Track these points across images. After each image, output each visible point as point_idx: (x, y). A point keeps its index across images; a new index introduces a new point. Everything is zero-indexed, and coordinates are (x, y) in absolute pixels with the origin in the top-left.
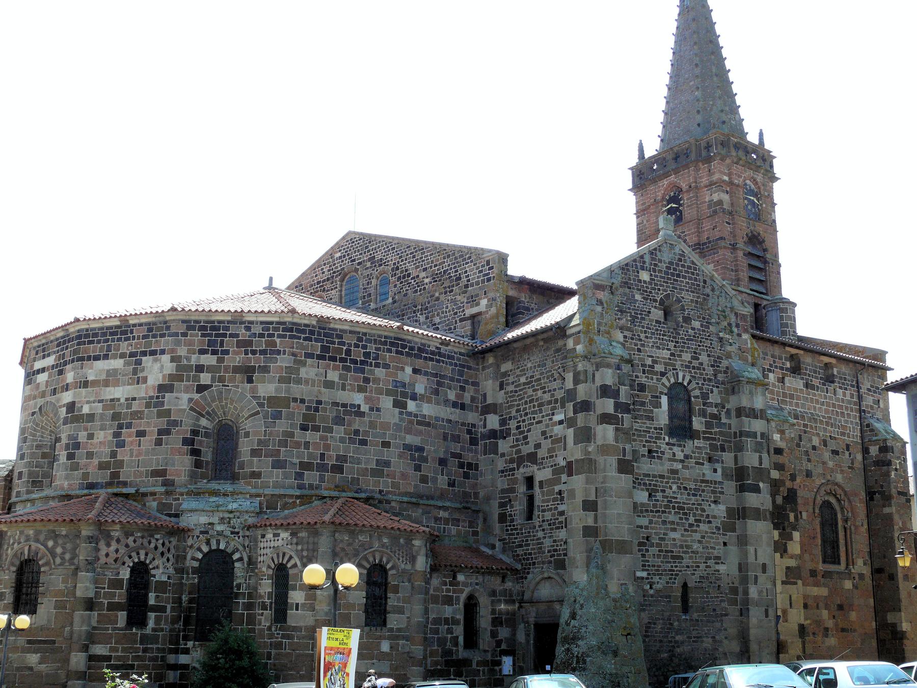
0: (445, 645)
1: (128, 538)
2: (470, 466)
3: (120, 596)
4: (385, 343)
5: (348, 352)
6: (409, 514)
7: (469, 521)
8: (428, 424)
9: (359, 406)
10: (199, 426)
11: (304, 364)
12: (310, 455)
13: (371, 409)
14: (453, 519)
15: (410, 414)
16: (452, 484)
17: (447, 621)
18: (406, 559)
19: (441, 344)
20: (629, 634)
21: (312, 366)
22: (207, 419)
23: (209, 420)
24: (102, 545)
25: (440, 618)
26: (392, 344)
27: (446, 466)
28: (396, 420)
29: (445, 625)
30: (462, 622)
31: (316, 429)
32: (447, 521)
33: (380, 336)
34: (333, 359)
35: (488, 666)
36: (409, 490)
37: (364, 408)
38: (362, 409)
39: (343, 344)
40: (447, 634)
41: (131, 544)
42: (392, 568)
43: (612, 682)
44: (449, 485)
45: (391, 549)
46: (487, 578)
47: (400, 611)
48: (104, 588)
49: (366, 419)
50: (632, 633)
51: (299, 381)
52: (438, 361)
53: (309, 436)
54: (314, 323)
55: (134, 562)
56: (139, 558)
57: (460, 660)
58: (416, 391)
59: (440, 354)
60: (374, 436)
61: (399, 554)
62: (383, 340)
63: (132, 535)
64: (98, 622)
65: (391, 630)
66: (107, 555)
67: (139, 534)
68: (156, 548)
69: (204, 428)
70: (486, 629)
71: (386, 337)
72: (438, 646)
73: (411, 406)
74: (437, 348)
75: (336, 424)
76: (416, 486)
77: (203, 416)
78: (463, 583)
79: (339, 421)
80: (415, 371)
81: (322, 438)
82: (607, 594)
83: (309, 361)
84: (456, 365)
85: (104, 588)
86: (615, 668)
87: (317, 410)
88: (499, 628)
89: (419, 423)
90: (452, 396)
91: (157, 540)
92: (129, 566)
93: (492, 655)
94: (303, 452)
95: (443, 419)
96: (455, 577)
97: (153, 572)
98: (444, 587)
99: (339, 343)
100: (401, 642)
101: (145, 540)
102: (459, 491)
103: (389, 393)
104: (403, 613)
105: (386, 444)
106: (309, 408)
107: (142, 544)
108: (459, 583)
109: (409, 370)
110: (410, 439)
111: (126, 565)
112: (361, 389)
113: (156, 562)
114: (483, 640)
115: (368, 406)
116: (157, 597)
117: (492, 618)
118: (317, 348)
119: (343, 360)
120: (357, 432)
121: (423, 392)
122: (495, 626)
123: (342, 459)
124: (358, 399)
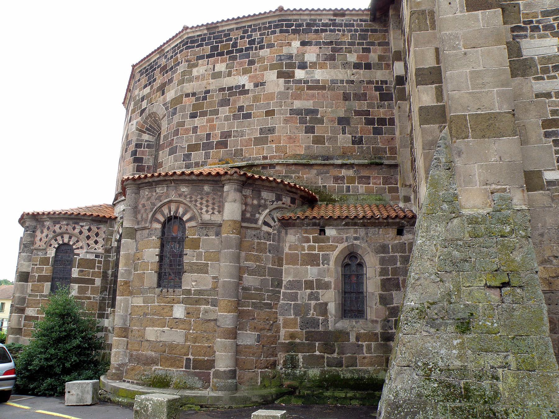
0: (307, 313)
1: (55, 226)
2: (382, 121)
3: (47, 270)
4: (270, 27)
5: (235, 45)
6: (299, 177)
7: (384, 178)
8: (323, 88)
9: (244, 86)
10: (142, 140)
11: (196, 65)
12: (198, 138)
13: (256, 85)
14: (361, 178)
15: (299, 81)
16: (357, 141)
17: (309, 284)
18: (213, 209)
19: (335, 15)
20: (505, 284)
21: (203, 65)
22: (148, 134)
23: (151, 135)
24: (38, 233)
25: (299, 282)
26: (276, 26)
27: (349, 124)
28: (282, 89)
29: (306, 289)
30: (333, 286)
31: (204, 114)
32: (351, 180)
33: (263, 24)
34: (221, 54)
35: (377, 340)
36: (298, 153)
37: (249, 86)
38: (246, 88)
39: (231, 40)
40: (310, 299)
41: (58, 230)
42: (190, 220)
43: (449, 386)
44: (354, 142)
45: (191, 198)
46: (372, 230)
47: (203, 269)
48: (36, 265)
49: (250, 95)
50: (514, 282)
51: (190, 80)
52: (331, 31)
53: (197, 121)
54: (206, 32)
55: (59, 244)
56: (63, 241)
57: (330, 332)
58: (305, 60)
59: (335, 25)
60: (258, 108)
61: (201, 204)
62: (267, 25)
63: (59, 223)
64: (32, 290)
65: (188, 292)
66: (41, 240)
67: (64, 222)
68: (81, 233)
69: (146, 141)
70: (373, 294)
71: (269, 23)
72: (296, 314)
73: (300, 74)
74: (331, 20)
75: (222, 106)
76: (308, 148)
77: (145, 132)
78: (334, 238)
79: (224, 102)
80: (303, 44)
81: (208, 121)
82: (456, 212)
83: (200, 62)
84: (356, 31)
85: (36, 265)
86: (460, 357)
87: (205, 98)
88: (394, 293)
89: (309, 88)
90: (352, 58)
91: (82, 226)
92: (54, 247)
93: (383, 327)
94: (191, 136)
95: (342, 82)
96: (322, 231)
97: (76, 251)
98: (306, 245)
99: (226, 41)
100: (203, 307)
101: (69, 227)
102: (369, 148)
103: (272, 67)
104: (207, 272)
105: (270, 113)
106: (198, 99)
107: (67, 230)
108: (328, 238)
109: (296, 44)
110: (298, 104)
111: (52, 246)
112: (245, 72)
113: (80, 244)
114: (371, 307)
115: (252, 84)
116: (81, 271)
117: (382, 280)
118: (207, 49)
119: (229, 53)
120: (241, 108)
121: (314, 60)
122: (386, 291)
123: (227, 135)
124: (243, 80)
